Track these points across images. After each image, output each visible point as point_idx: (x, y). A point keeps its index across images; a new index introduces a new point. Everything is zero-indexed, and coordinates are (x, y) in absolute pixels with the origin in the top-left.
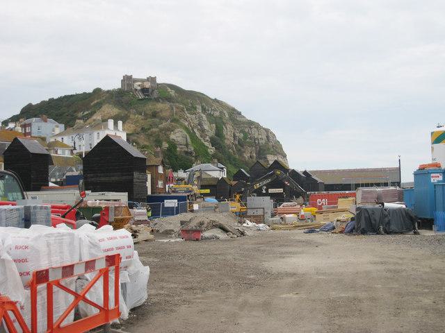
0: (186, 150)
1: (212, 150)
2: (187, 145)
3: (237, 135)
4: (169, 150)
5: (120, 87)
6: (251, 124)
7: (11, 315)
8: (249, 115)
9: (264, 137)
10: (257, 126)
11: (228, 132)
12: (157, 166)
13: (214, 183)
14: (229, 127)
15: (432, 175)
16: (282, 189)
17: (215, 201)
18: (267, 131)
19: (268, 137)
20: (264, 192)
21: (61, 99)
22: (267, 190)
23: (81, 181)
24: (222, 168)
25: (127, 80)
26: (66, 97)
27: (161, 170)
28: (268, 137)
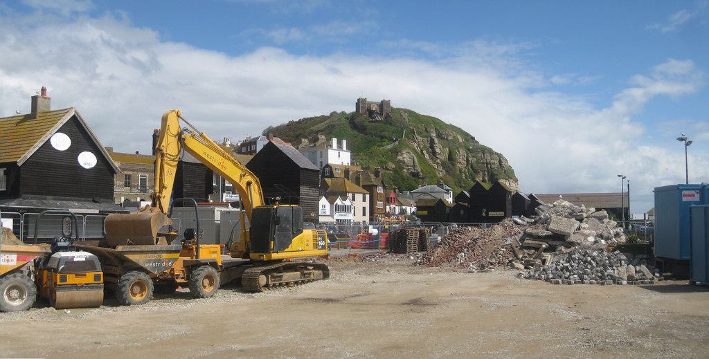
0: (413, 171)
1: (441, 173)
2: (414, 166)
3: (470, 159)
4: (395, 171)
5: (355, 110)
6: (485, 150)
7: (353, 300)
8: (483, 140)
9: (497, 162)
10: (490, 152)
11: (461, 156)
12: (376, 186)
13: (432, 204)
14: (462, 151)
15: (684, 192)
16: (503, 213)
17: (308, 233)
18: (500, 156)
19: (500, 162)
20: (484, 214)
21: (299, 122)
22: (487, 213)
23: (404, 207)
24: (448, 190)
25: (360, 103)
26: (305, 119)
27: (380, 190)
28: (500, 162)
